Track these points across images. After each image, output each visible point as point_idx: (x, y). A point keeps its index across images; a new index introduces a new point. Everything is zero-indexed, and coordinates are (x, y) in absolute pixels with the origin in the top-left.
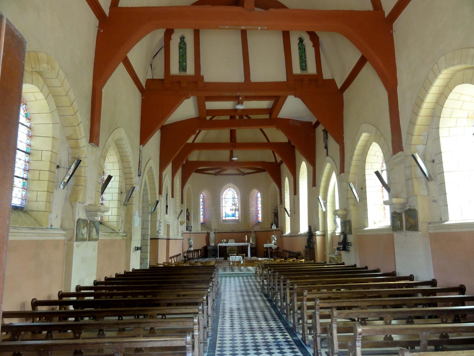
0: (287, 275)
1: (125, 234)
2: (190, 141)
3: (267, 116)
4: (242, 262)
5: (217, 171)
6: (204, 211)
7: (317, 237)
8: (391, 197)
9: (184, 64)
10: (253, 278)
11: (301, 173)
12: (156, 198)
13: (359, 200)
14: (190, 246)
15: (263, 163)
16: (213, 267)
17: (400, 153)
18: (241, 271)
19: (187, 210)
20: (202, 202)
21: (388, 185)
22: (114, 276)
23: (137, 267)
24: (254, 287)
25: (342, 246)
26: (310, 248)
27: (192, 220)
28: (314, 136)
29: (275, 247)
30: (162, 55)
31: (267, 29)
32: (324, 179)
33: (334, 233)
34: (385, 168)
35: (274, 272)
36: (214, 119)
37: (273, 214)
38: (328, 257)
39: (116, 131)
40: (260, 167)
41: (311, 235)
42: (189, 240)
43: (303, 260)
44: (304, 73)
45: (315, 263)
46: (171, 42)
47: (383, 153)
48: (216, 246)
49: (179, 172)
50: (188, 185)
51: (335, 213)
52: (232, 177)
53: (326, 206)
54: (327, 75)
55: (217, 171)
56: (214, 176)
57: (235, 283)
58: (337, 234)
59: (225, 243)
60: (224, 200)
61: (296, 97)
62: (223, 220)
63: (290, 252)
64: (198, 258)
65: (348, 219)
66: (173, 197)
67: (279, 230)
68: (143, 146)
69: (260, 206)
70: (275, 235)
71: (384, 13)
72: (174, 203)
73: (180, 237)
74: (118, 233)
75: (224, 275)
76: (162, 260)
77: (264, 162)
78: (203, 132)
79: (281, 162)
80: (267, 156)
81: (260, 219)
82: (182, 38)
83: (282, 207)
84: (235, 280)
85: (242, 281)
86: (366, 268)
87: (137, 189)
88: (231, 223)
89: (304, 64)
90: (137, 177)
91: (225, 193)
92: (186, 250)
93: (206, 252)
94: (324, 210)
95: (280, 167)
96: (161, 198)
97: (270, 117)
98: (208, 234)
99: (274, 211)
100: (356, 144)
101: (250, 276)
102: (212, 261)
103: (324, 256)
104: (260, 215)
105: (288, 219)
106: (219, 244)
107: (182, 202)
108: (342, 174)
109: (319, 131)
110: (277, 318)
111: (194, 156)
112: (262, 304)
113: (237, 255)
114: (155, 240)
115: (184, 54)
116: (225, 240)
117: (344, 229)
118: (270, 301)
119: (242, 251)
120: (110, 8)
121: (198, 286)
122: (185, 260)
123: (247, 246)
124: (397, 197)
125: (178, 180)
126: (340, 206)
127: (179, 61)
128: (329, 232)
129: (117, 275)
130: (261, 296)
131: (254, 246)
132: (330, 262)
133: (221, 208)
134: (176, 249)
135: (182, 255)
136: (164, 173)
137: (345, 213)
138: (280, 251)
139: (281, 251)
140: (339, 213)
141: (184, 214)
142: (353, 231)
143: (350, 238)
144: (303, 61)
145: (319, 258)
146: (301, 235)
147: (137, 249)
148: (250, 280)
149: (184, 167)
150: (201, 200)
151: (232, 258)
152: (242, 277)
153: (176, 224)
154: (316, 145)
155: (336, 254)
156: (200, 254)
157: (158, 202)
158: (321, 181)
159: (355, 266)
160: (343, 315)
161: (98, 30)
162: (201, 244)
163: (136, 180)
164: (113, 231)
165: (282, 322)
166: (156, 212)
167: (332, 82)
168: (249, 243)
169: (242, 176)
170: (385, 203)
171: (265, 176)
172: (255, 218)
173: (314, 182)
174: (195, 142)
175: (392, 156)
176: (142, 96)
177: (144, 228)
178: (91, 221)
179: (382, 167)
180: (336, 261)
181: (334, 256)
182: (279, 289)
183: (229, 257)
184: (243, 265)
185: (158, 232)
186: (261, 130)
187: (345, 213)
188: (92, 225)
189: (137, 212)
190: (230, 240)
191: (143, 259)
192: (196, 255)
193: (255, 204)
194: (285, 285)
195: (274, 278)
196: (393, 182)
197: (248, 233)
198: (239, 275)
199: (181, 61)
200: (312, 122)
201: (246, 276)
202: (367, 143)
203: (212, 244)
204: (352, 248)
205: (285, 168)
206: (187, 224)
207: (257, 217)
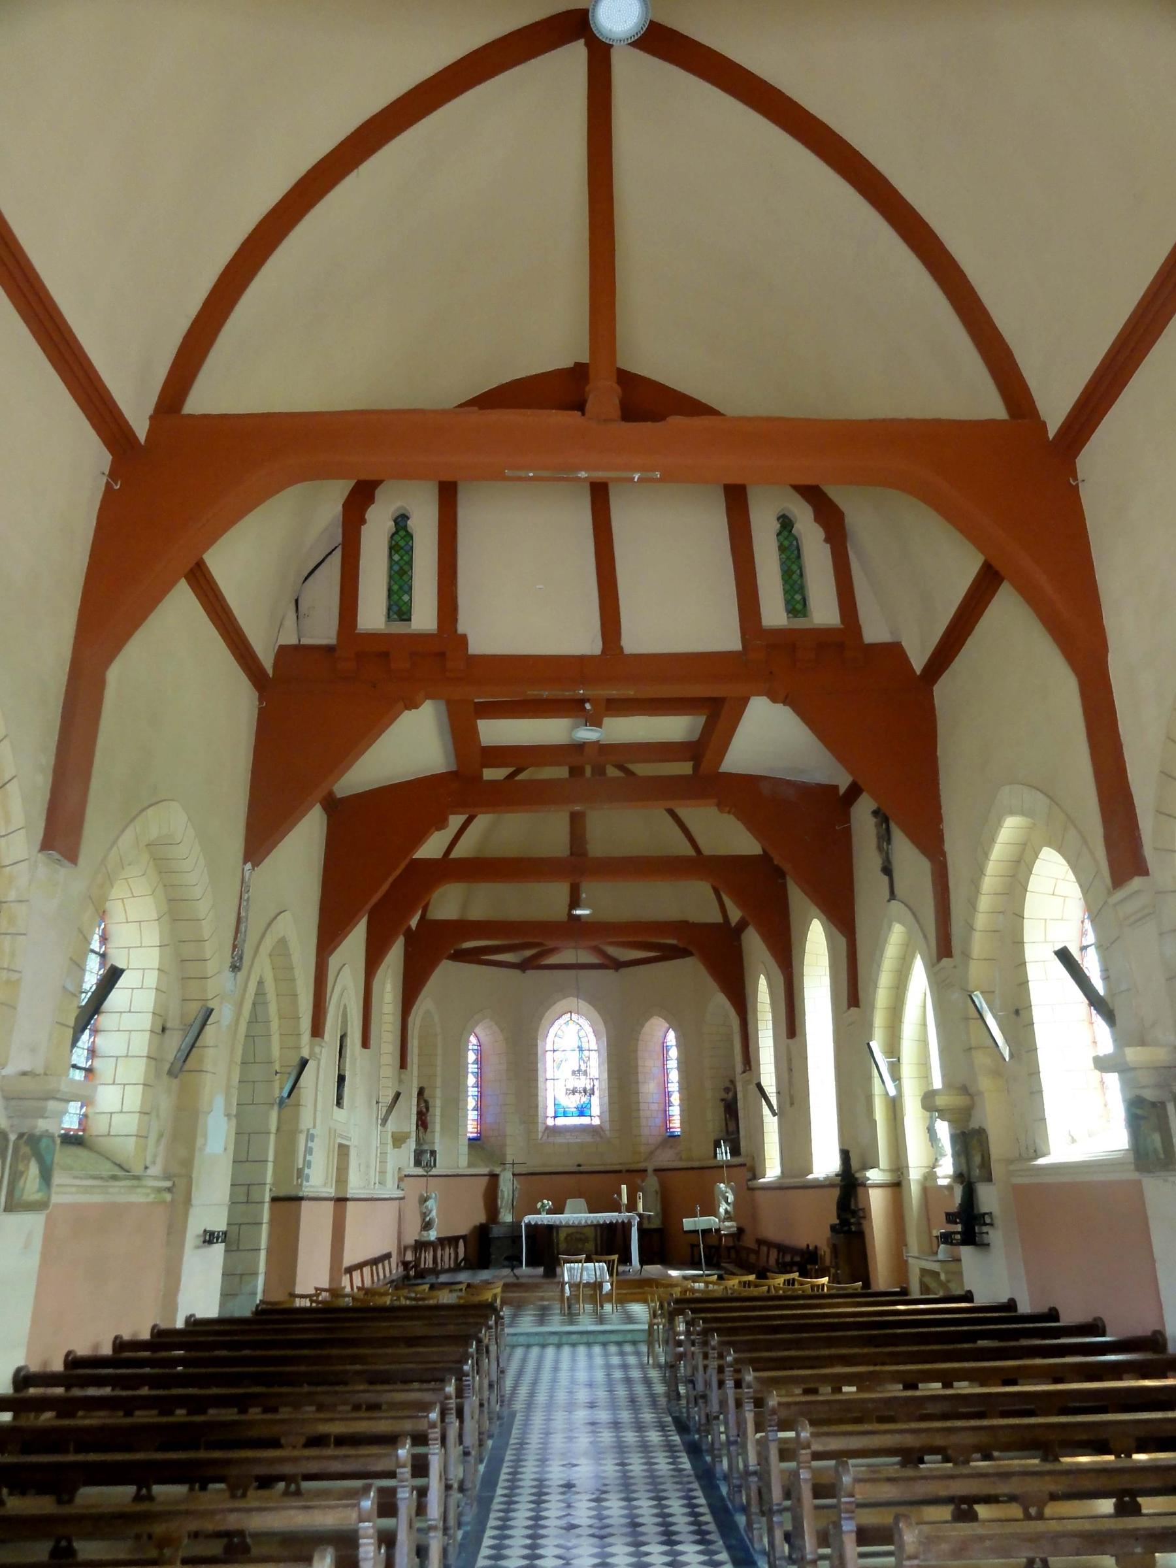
0: (753, 1346)
1: (168, 1184)
2: (432, 848)
3: (684, 768)
4: (607, 1287)
5: (528, 953)
6: (481, 1097)
7: (871, 1191)
8: (1120, 1041)
9: (406, 598)
11: (808, 959)
12: (298, 1048)
13: (1012, 1055)
14: (427, 1226)
15: (681, 927)
16: (489, 1308)
17: (1137, 883)
18: (601, 1320)
19: (421, 1092)
20: (476, 1062)
21: (1109, 1001)
22: (107, 1350)
23: (208, 1308)
24: (640, 1390)
25: (959, 1228)
26: (849, 1232)
27: (438, 1127)
28: (847, 834)
29: (729, 1226)
30: (333, 570)
31: (662, 480)
33: (930, 1176)
34: (1091, 938)
35: (705, 1332)
36: (520, 777)
37: (722, 1104)
38: (916, 1266)
39: (150, 811)
40: (668, 942)
41: (849, 1184)
42: (424, 1200)
43: (825, 1280)
44: (800, 623)
45: (868, 1294)
46: (365, 530)
47: (1081, 886)
48: (516, 1225)
49: (395, 956)
50: (425, 1004)
51: (929, 1101)
53: (896, 1077)
54: (874, 632)
55: (528, 953)
57: (573, 1369)
58: (943, 1182)
59: (549, 1212)
60: (549, 1055)
61: (774, 700)
62: (547, 1128)
63: (782, 1249)
64: (457, 1268)
65: (974, 1124)
66: (365, 1044)
68: (256, 864)
69: (674, 1076)
71: (1043, 426)
72: (372, 1071)
73: (390, 1189)
74: (137, 1178)
75: (536, 1340)
76: (312, 1278)
77: (686, 922)
78: (482, 821)
79: (742, 925)
80: (696, 901)
81: (676, 1124)
82: (401, 521)
83: (748, 1082)
84: (573, 1359)
85: (599, 1361)
86: (1053, 1315)
87: (224, 1014)
88: (570, 1139)
89: (798, 597)
90: (228, 974)
93: (485, 1246)
96: (317, 1050)
97: (696, 768)
98: (494, 1177)
99: (725, 1096)
100: (986, 855)
101: (634, 1343)
102: (493, 1282)
103: (900, 1265)
104: (675, 1111)
105: (771, 1126)
106: (528, 1219)
107: (403, 1065)
108: (945, 961)
109: (863, 813)
110: (712, 1527)
111: (448, 903)
112: (663, 1464)
113: (588, 1260)
114: (288, 1202)
115: (406, 568)
116: (548, 1203)
117: (963, 1160)
118: (694, 1450)
119: (608, 1243)
120: (151, 418)
121: (399, 1397)
122: (406, 1277)
124: (1142, 1043)
125: (389, 987)
126: (944, 1076)
127: (390, 590)
128: (915, 1174)
129: (120, 1345)
130: (662, 1427)
131: (656, 1224)
132: (925, 1288)
133: (541, 1085)
134: (373, 1237)
135: (394, 1260)
136: (334, 961)
138: (749, 1242)
139: (753, 1246)
140: (940, 1101)
141: (409, 1106)
142: (997, 1170)
143: (989, 1198)
144: (796, 587)
145: (882, 1277)
146: (818, 1185)
147: (210, 1238)
149: (411, 939)
150: (471, 1057)
151: (570, 1269)
153: (375, 1142)
154: (855, 861)
155: (941, 1256)
156: (461, 1255)
157: (304, 1063)
158: (876, 987)
159: (1011, 1305)
160: (944, 1547)
161: (108, 483)
162: (465, 1218)
163: (220, 984)
164: (122, 1171)
165: (729, 1548)
166: (299, 1095)
167: (894, 651)
168: (633, 1213)
169: (611, 972)
170: (1102, 1064)
171: (690, 973)
172: (659, 1121)
173: (852, 992)
174: (454, 855)
175: (1110, 894)
176: (261, 700)
177: (245, 1155)
178: (21, 1136)
179: (1083, 933)
180: (943, 1285)
181: (936, 1267)
182: (723, 1403)
183: (559, 1265)
184: (609, 1298)
185: (300, 1173)
186: (672, 813)
188: (25, 1149)
189: (219, 1103)
190: (570, 1203)
191: (234, 1279)
192: (447, 1257)
193: (656, 1071)
194: (738, 1384)
195: (706, 1356)
196: (1124, 987)
197: (633, 1175)
198: (591, 1338)
199: (395, 587)
200: (836, 788)
201: (619, 1344)
202: (1024, 849)
203: (507, 1217)
204: (995, 1236)
205: (754, 944)
206: (418, 1142)
207: (666, 1118)
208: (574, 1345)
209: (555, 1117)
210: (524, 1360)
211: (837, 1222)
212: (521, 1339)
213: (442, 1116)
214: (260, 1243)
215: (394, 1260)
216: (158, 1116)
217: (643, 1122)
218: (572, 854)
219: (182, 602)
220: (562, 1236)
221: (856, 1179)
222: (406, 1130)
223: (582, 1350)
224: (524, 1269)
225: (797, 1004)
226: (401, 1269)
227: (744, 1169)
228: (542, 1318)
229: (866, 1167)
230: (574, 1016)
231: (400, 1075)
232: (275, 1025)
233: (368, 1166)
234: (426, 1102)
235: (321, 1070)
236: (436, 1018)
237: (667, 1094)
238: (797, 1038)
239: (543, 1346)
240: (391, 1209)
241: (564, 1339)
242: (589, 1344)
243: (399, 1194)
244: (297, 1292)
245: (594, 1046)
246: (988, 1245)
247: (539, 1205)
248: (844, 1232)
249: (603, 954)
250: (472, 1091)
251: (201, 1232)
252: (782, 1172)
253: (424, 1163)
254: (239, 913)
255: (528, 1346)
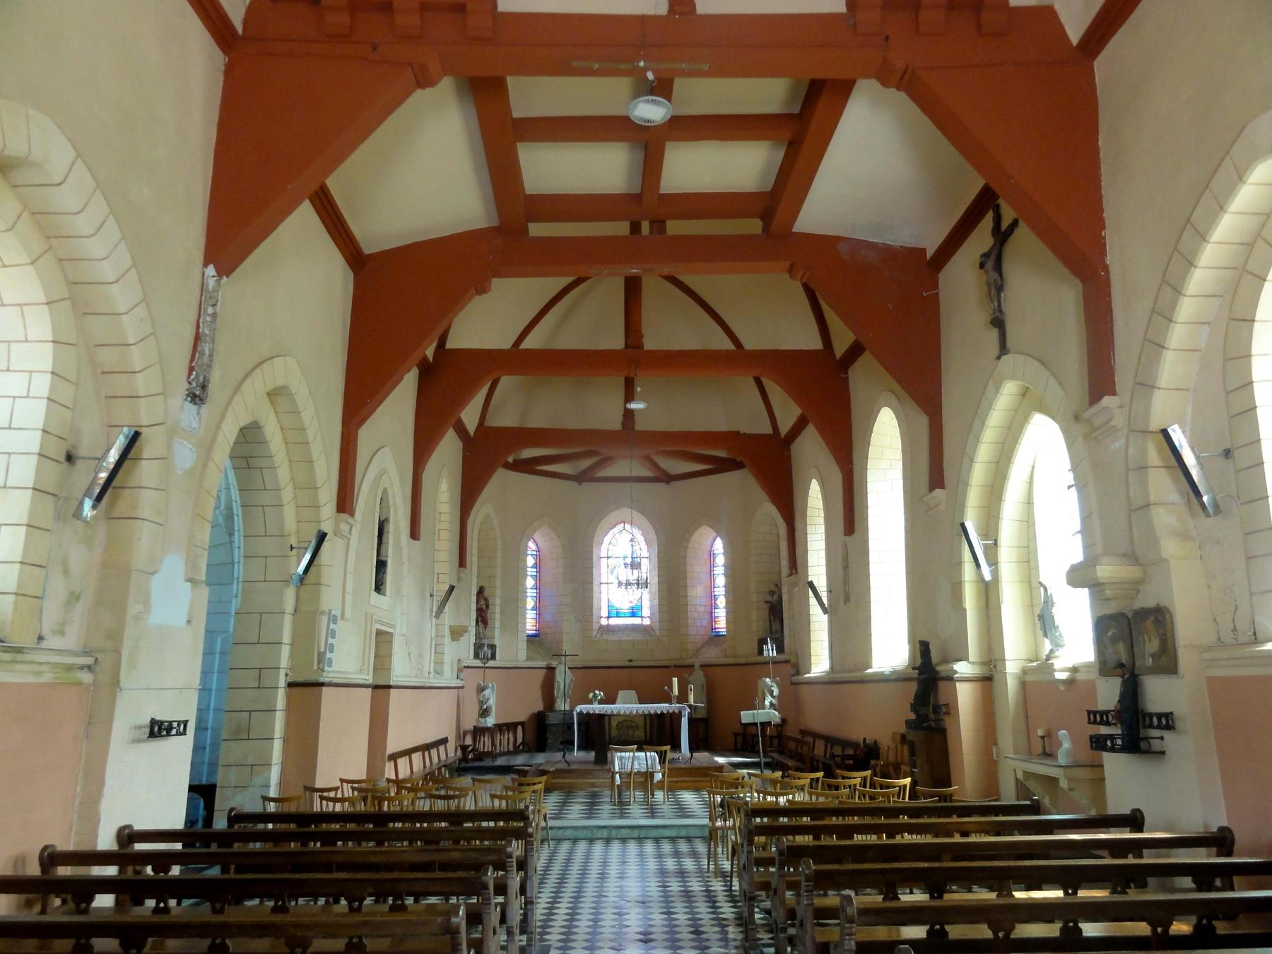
1: (88, 661)
3: (754, 226)
4: (658, 777)
5: (585, 464)
6: (539, 597)
7: (959, 686)
10: (701, 848)
14: (484, 713)
15: (731, 438)
18: (652, 811)
19: (481, 591)
20: (535, 566)
24: (703, 910)
27: (497, 624)
32: (984, 453)
37: (767, 606)
41: (928, 676)
42: (481, 689)
49: (448, 451)
50: (483, 509)
52: (627, 485)
53: (993, 562)
56: (574, 484)
60: (604, 561)
62: (601, 627)
64: (516, 751)
66: (414, 534)
67: (787, 662)
69: (720, 581)
70: (773, 679)
73: (449, 678)
81: (722, 625)
85: (652, 865)
91: (607, 539)
92: (469, 725)
93: (542, 731)
94: (988, 577)
95: (789, 449)
97: (766, 229)
98: (551, 670)
99: (770, 599)
101: (689, 839)
103: (990, 766)
105: (819, 623)
106: (578, 709)
107: (462, 563)
119: (659, 733)
123: (679, 715)
125: (444, 487)
133: (595, 588)
134: (422, 723)
136: (367, 435)
137: (1128, 572)
138: (791, 731)
142: (1185, 658)
143: (1159, 694)
146: (881, 679)
148: (689, 864)
149: (427, 372)
150: (530, 561)
152: (657, 840)
156: (520, 740)
157: (322, 537)
162: (526, 706)
166: (319, 575)
168: (684, 704)
171: (740, 486)
172: (705, 622)
173: (934, 471)
184: (660, 786)
185: (321, 657)
187: (1128, 572)
190: (621, 693)
192: (505, 741)
197: (682, 669)
200: (924, 250)
201: (673, 840)
203: (561, 705)
205: (811, 449)
207: (712, 619)
208: (624, 840)
209: (608, 617)
210: (568, 861)
211: (913, 716)
212: (568, 833)
213: (503, 612)
214: (273, 732)
215: (451, 745)
216: (66, 572)
217: (690, 621)
218: (627, 346)
219: (304, 217)
220: (614, 723)
221: (937, 673)
222: (466, 624)
223: (632, 847)
224: (577, 754)
225: (856, 501)
226: (459, 753)
227: (788, 666)
228: (592, 808)
229: (949, 659)
230: (628, 527)
231: (459, 572)
232: (287, 495)
233: (420, 656)
234: (486, 600)
235: (351, 550)
236: (496, 523)
237: (713, 598)
238: (857, 534)
239: (591, 841)
240: (449, 698)
241: (614, 832)
242: (640, 840)
243: (460, 683)
244: (317, 786)
245: (645, 553)
246: (1163, 753)
247: (591, 695)
248: (925, 728)
249: (656, 466)
250: (531, 593)
251: (147, 722)
252: (832, 667)
253: (481, 655)
254: (198, 327)
255: (575, 841)
